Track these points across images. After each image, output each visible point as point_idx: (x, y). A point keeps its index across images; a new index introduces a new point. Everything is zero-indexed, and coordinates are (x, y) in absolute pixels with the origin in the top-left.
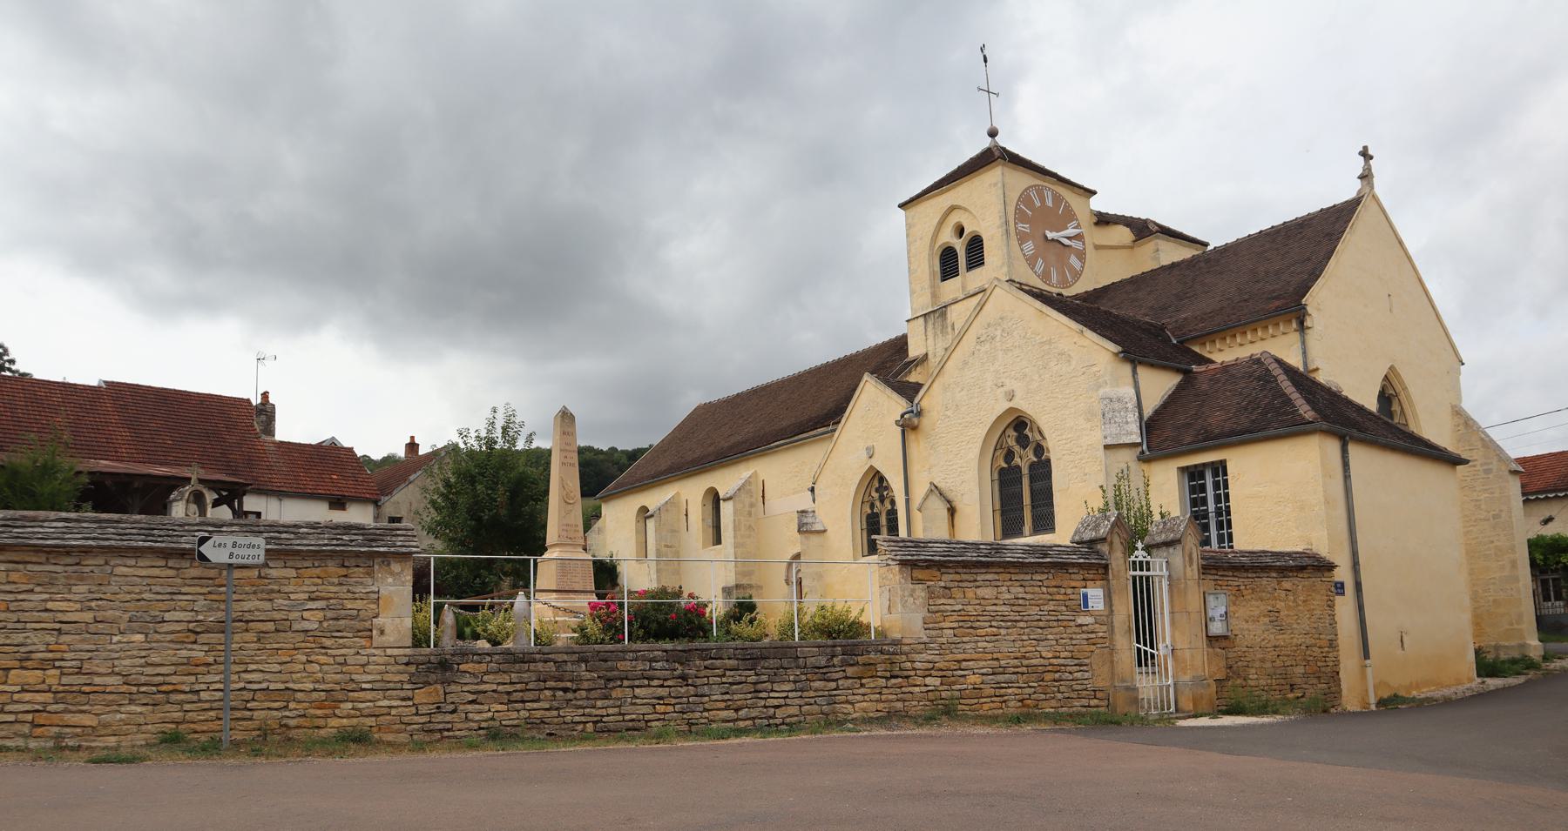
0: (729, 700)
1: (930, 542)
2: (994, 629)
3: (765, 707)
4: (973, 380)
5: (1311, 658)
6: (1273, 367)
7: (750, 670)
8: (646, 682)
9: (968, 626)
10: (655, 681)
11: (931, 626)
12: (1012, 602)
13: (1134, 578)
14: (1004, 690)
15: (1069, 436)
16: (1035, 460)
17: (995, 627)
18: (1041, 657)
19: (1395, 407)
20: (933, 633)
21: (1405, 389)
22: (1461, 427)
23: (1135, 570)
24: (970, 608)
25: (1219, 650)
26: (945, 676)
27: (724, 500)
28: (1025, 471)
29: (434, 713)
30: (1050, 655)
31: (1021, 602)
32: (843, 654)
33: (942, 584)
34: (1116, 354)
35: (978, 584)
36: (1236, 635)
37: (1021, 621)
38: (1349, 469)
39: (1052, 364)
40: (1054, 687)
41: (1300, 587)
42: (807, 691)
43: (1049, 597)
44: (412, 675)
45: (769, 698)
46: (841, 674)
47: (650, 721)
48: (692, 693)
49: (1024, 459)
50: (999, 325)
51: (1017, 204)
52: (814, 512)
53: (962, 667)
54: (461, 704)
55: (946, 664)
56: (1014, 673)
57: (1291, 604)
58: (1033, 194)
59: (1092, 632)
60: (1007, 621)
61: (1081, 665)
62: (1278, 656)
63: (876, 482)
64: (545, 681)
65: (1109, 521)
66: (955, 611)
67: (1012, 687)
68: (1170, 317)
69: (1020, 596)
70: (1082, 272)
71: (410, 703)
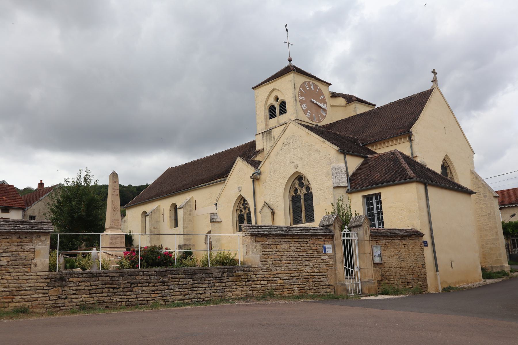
1: (263, 226)
2: (288, 261)
3: (196, 294)
4: (281, 160)
5: (415, 272)
8: (147, 284)
9: (278, 260)
10: (151, 284)
11: (263, 260)
12: (295, 250)
13: (344, 240)
14: (293, 286)
15: (319, 183)
18: (307, 272)
21: (452, 164)
24: (279, 253)
25: (378, 269)
26: (269, 280)
28: (302, 197)
29: (57, 299)
30: (311, 271)
31: (299, 250)
33: (268, 243)
34: (338, 151)
35: (282, 243)
36: (385, 263)
38: (428, 196)
39: (313, 154)
42: (213, 287)
44: (48, 283)
45: (198, 290)
47: (149, 300)
49: (302, 192)
50: (292, 138)
51: (300, 89)
52: (217, 214)
54: (69, 295)
55: (269, 275)
56: (296, 279)
58: (306, 85)
59: (328, 262)
62: (402, 271)
63: (242, 201)
64: (105, 285)
67: (296, 285)
68: (360, 135)
69: (299, 248)
70: (326, 116)
71: (47, 295)
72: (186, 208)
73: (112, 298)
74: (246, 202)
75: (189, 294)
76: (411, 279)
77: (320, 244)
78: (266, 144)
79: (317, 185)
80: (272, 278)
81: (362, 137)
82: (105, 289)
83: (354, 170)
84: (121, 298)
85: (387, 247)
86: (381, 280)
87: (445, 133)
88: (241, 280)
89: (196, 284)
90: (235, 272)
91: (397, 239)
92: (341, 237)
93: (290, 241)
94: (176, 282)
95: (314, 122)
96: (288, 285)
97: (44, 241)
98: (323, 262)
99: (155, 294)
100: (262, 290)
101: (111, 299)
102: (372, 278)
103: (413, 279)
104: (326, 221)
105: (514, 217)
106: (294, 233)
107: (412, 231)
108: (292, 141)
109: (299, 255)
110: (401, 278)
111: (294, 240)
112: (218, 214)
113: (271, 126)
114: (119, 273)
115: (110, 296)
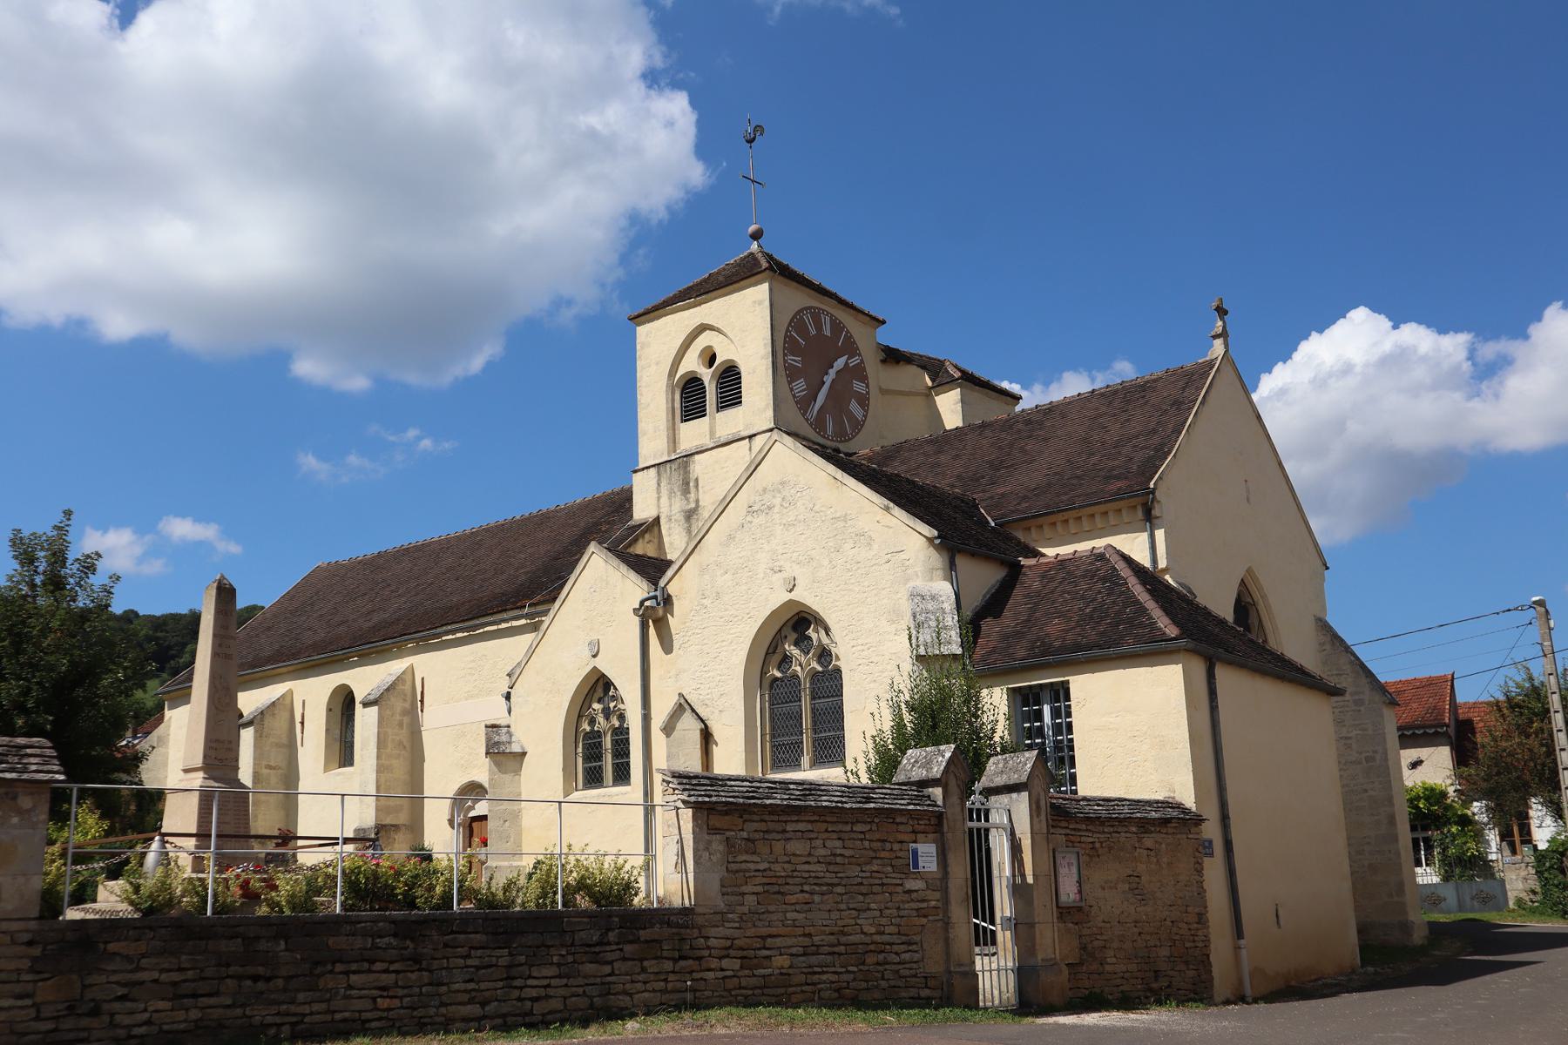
0: (474, 990)
1: (730, 780)
2: (807, 896)
3: (520, 999)
4: (741, 561)
5: (1177, 937)
6: (1120, 565)
7: (503, 948)
8: (366, 965)
9: (775, 890)
10: (378, 964)
11: (729, 890)
12: (828, 859)
13: (971, 830)
14: (817, 976)
16: (820, 669)
17: (807, 892)
18: (863, 933)
19: (1253, 620)
20: (732, 898)
21: (1264, 597)
22: (1328, 647)
23: (971, 819)
24: (777, 867)
25: (1071, 925)
26: (745, 958)
27: (366, 704)
29: (64, 1016)
30: (873, 930)
31: (839, 859)
32: (620, 927)
33: (745, 835)
34: (930, 540)
35: (788, 835)
36: (1091, 906)
37: (839, 885)
38: (1216, 697)
39: (847, 546)
40: (878, 972)
41: (1163, 846)
42: (574, 977)
43: (872, 854)
44: (34, 959)
45: (527, 986)
46: (617, 955)
47: (369, 1021)
48: (426, 981)
49: (803, 664)
51: (787, 330)
52: (509, 727)
53: (767, 946)
54: (105, 1001)
55: (748, 940)
56: (829, 954)
57: (1153, 866)
58: (807, 319)
59: (923, 901)
60: (822, 885)
61: (910, 944)
62: (1140, 934)
63: (598, 686)
64: (228, 965)
65: (943, 757)
66: (759, 871)
67: (827, 972)
68: (984, 491)
69: (838, 852)
70: (864, 422)
71: (28, 1002)
72: (388, 702)
73: (247, 1013)
74: (611, 693)
75: (499, 998)
76: (1165, 961)
77: (901, 842)
78: (668, 504)
79: (860, 648)
80: (755, 950)
81: (992, 498)
82: (229, 981)
83: (976, 604)
84: (278, 1014)
85: (1098, 856)
86: (1077, 962)
87: (1248, 500)
88: (659, 954)
89: (522, 965)
90: (642, 929)
91: (1126, 832)
92: (964, 819)
93: (812, 831)
94: (456, 957)
95: (828, 439)
96: (802, 973)
97: (29, 811)
98: (909, 900)
99: (388, 1000)
100: (725, 990)
101: (244, 1014)
102: (1053, 956)
103: (1172, 959)
104: (919, 767)
105: (1419, 768)
106: (824, 804)
107: (1170, 807)
108: (780, 499)
109: (839, 875)
110: (1136, 957)
111: (824, 826)
112: (512, 729)
113: (685, 445)
114: (275, 925)
115: (243, 1006)
